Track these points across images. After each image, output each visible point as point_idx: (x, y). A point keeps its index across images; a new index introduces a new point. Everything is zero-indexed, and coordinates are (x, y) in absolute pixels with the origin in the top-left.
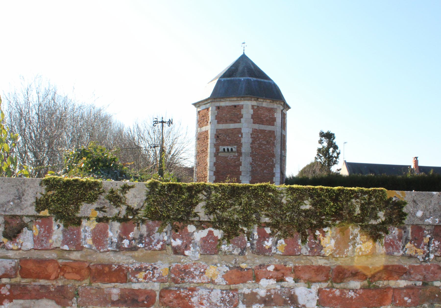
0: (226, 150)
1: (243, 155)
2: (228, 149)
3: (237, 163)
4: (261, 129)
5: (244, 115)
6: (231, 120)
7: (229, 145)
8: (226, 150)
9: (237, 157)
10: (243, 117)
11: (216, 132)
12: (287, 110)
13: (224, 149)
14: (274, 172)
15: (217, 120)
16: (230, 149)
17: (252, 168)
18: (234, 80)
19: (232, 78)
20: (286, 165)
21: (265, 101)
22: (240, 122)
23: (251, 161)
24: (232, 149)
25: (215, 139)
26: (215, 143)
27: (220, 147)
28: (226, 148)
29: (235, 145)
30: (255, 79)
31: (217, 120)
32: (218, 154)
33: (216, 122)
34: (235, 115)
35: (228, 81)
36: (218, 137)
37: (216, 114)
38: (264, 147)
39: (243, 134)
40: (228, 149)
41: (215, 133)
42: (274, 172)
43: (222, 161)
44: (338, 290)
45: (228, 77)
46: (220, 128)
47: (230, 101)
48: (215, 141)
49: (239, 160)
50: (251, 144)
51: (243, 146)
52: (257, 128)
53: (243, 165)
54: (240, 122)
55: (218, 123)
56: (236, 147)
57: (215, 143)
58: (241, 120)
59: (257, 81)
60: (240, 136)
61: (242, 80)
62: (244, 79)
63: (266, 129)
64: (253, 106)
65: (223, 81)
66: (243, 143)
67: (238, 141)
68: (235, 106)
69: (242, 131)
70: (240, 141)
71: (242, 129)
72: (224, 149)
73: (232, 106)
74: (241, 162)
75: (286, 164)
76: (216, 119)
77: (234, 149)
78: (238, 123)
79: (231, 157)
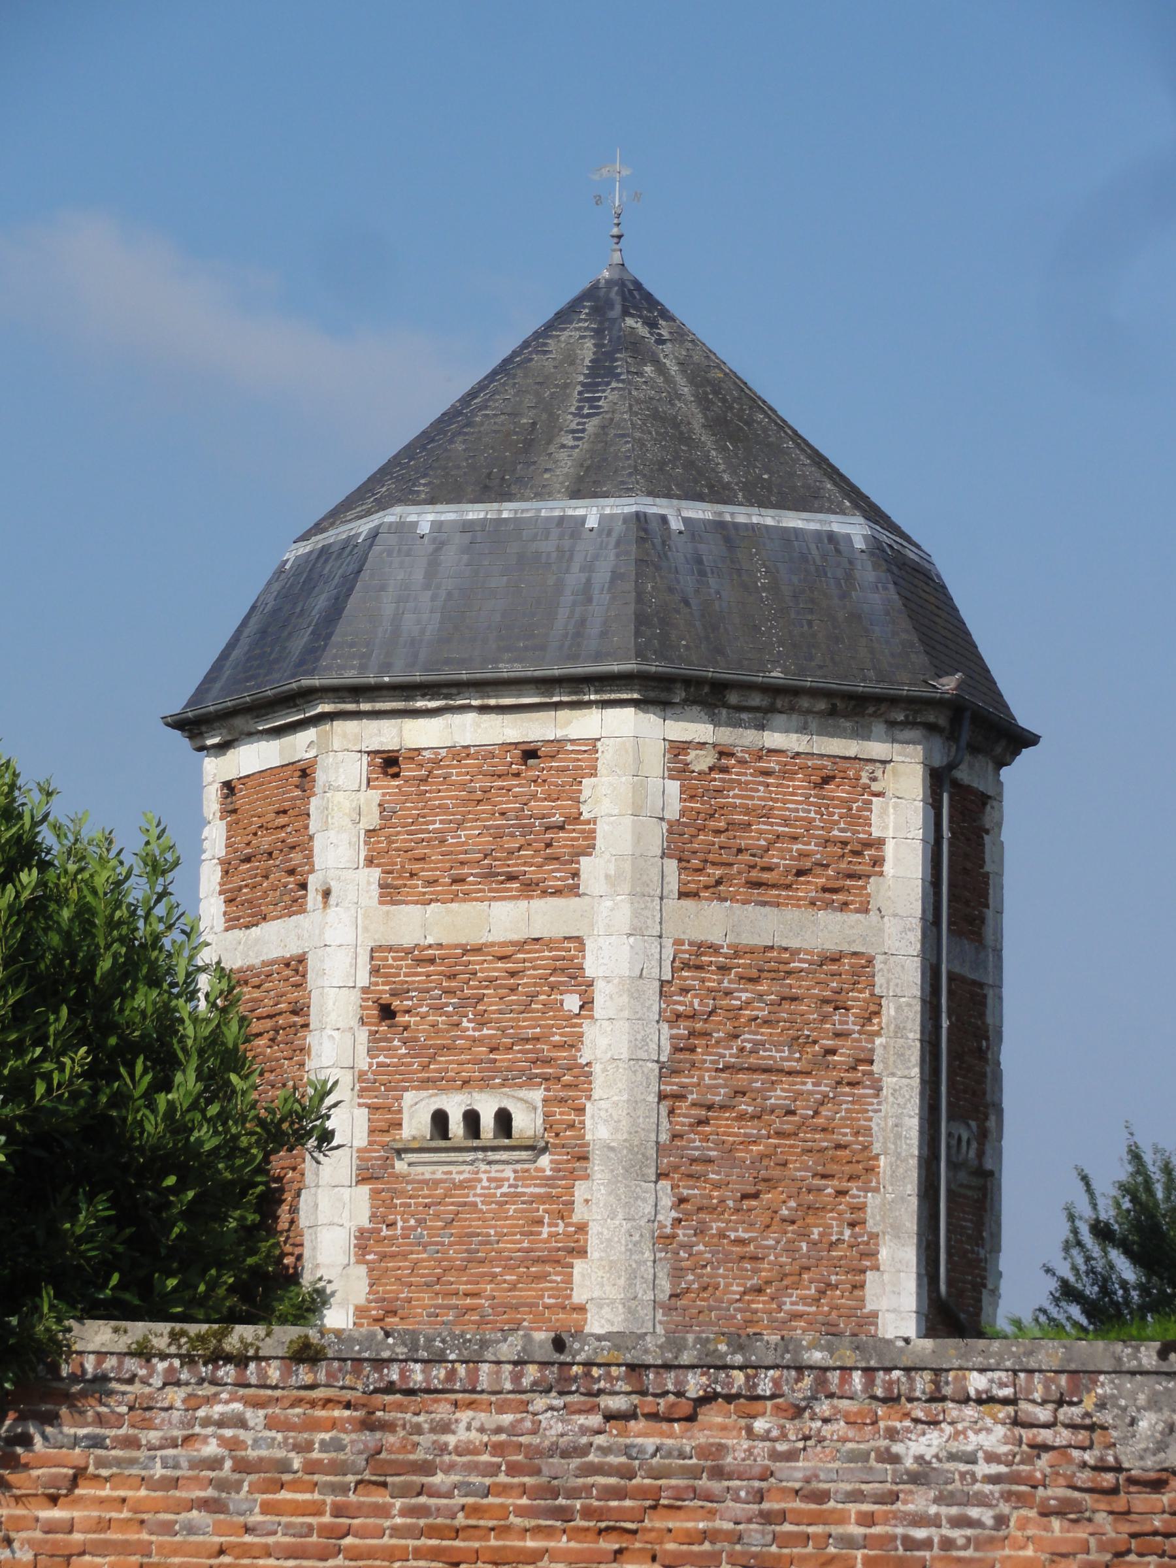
0: (456, 1126)
1: (597, 1167)
2: (472, 1119)
3: (545, 1231)
4: (748, 939)
5: (602, 829)
6: (490, 875)
7: (484, 1084)
8: (456, 1126)
9: (548, 1181)
10: (599, 843)
11: (375, 971)
12: (1001, 763)
13: (440, 1120)
14: (870, 1307)
15: (376, 873)
16: (487, 1122)
17: (677, 1273)
18: (517, 523)
19: (507, 510)
20: (996, 1249)
21: (779, 704)
22: (573, 890)
23: (667, 1216)
24: (504, 1120)
25: (363, 1035)
26: (363, 1063)
27: (409, 1097)
28: (455, 1106)
29: (530, 1081)
30: (701, 512)
31: (376, 873)
32: (387, 1163)
33: (375, 891)
34: (526, 829)
35: (467, 527)
36: (387, 1013)
37: (372, 819)
38: (778, 1096)
39: (599, 986)
40: (472, 1119)
41: (363, 979)
42: (870, 1307)
43: (420, 1222)
44: (275, 1363)
45: (95, 1532)
46: (408, 941)
47: (484, 709)
48: (362, 1049)
49: (564, 1211)
50: (668, 1071)
51: (596, 1095)
52: (715, 938)
53: (594, 1251)
54: (573, 890)
55: (390, 893)
56: (537, 1095)
57: (363, 1063)
58: (575, 874)
59: (720, 526)
60: (572, 1003)
61: (592, 522)
62: (603, 518)
63: (794, 944)
64: (678, 749)
65: (424, 528)
66: (597, 1068)
67: (557, 1046)
68: (530, 753)
69: (591, 969)
70: (574, 1044)
71: (589, 945)
72: (440, 1120)
73: (507, 746)
74: (582, 1228)
75: (996, 1236)
76: (370, 862)
77: (525, 1123)
78: (558, 892)
79: (499, 1181)
